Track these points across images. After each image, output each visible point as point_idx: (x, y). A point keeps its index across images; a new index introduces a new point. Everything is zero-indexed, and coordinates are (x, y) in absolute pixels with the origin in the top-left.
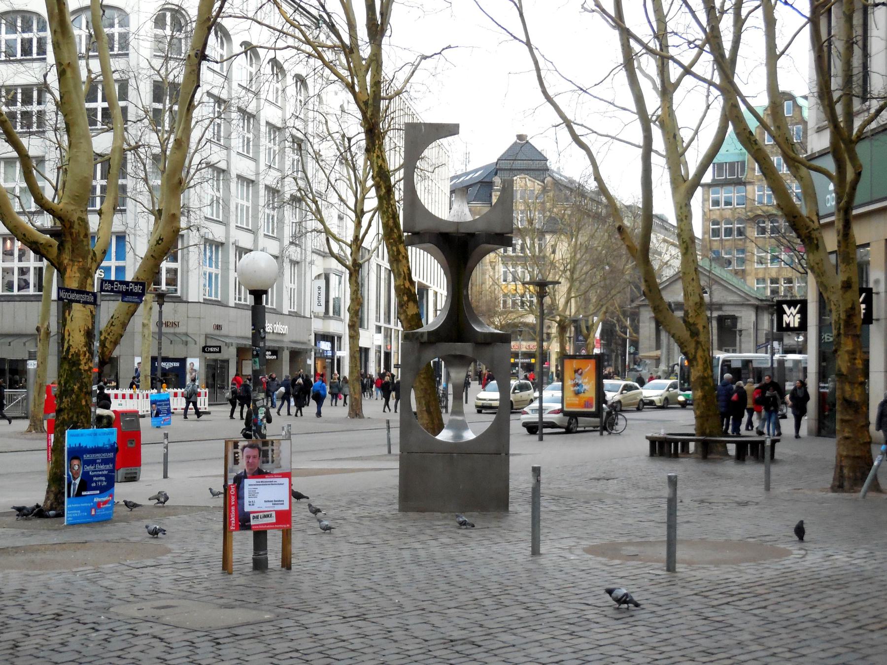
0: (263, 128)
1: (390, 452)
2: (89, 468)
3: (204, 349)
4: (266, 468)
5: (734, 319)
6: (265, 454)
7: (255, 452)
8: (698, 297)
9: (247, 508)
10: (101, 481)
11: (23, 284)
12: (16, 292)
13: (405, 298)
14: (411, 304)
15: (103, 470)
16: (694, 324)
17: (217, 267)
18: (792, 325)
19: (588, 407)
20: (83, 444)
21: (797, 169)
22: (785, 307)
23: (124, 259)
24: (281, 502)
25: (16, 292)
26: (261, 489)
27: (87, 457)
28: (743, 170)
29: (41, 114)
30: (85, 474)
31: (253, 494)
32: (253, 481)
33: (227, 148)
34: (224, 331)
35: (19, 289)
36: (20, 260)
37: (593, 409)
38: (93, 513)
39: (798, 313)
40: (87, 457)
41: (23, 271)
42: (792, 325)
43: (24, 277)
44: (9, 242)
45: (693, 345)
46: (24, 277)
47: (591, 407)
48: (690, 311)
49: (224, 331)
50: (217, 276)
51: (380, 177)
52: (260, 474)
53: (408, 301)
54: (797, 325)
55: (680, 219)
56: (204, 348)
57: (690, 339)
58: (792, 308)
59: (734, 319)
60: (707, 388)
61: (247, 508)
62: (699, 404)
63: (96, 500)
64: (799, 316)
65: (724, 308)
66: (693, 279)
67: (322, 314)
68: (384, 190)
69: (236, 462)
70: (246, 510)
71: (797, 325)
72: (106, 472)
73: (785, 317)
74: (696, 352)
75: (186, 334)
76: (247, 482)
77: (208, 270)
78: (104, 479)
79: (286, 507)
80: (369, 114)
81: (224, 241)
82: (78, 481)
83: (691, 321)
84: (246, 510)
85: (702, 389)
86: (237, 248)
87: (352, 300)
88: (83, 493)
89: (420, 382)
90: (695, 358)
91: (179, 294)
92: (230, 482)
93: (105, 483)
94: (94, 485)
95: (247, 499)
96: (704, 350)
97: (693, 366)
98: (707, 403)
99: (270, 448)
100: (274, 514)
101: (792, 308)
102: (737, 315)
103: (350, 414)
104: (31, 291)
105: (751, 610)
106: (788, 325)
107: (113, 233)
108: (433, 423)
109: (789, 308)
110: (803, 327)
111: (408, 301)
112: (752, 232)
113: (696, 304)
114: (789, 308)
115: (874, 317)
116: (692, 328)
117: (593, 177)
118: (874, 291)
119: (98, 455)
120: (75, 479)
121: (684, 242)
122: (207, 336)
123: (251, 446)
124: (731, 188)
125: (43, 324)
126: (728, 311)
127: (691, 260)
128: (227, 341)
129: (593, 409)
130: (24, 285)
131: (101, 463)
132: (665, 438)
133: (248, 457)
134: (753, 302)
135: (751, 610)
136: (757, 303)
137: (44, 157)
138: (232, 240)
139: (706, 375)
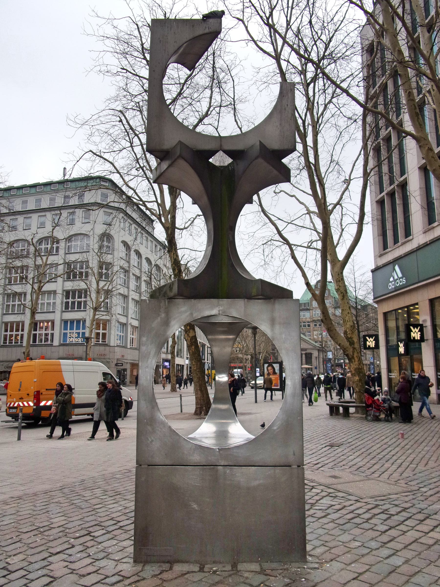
1: (182, 411)
3: (116, 365)
5: (311, 354)
8: (352, 322)
11: (46, 340)
12: (43, 343)
13: (188, 328)
14: (191, 331)
16: (351, 338)
17: (123, 333)
18: (371, 346)
19: (276, 386)
22: (367, 338)
25: (43, 343)
28: (308, 306)
33: (128, 288)
34: (125, 358)
35: (45, 342)
36: (46, 330)
37: (279, 387)
39: (374, 340)
41: (46, 335)
42: (371, 346)
43: (47, 337)
44: (42, 324)
45: (351, 350)
46: (47, 337)
47: (278, 386)
48: (348, 331)
49: (125, 358)
50: (123, 336)
51: (175, 265)
53: (190, 329)
54: (373, 346)
56: (116, 364)
57: (349, 347)
58: (371, 338)
59: (311, 354)
60: (361, 375)
62: (357, 384)
64: (374, 342)
65: (308, 350)
66: (348, 313)
67: (165, 352)
68: (177, 271)
71: (373, 346)
73: (368, 342)
74: (353, 354)
75: (109, 359)
77: (119, 334)
80: (169, 232)
81: (125, 322)
83: (349, 336)
85: (359, 375)
86: (131, 326)
87: (172, 342)
89: (196, 373)
90: (353, 357)
91: (107, 343)
96: (358, 353)
97: (352, 362)
98: (362, 383)
101: (371, 338)
102: (312, 352)
103: (171, 390)
104: (49, 342)
106: (369, 346)
108: (203, 397)
109: (369, 338)
110: (377, 346)
111: (190, 329)
113: (351, 326)
114: (369, 338)
115: (425, 339)
116: (350, 340)
117: (291, 257)
118: (424, 325)
121: (341, 293)
122: (118, 360)
124: (305, 311)
125: (26, 351)
126: (308, 351)
127: (346, 302)
128: (126, 361)
129: (279, 387)
130: (46, 340)
132: (402, 416)
134: (317, 348)
136: (319, 348)
137: (56, 291)
138: (129, 323)
139: (360, 367)
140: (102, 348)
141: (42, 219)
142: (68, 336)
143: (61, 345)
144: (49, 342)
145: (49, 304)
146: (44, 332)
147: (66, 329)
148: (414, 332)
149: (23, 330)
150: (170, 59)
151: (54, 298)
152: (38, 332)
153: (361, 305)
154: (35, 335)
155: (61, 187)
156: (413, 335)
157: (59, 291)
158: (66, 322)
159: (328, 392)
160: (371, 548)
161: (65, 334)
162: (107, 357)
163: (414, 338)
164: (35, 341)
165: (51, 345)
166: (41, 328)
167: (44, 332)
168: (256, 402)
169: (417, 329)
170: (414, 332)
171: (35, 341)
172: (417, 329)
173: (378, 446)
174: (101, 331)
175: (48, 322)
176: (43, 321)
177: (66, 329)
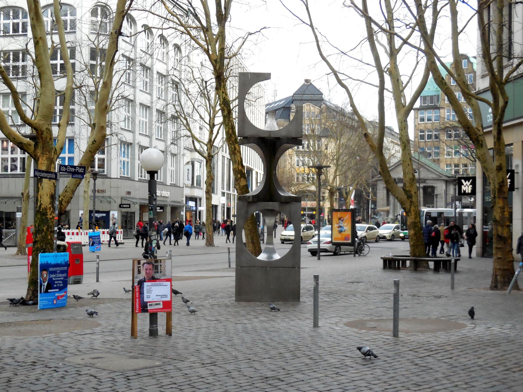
0: (155, 76)
1: (230, 266)
2: (52, 276)
3: (121, 206)
4: (157, 276)
5: (433, 188)
6: (156, 268)
7: (150, 266)
8: (412, 175)
9: (146, 300)
10: (60, 284)
11: (14, 167)
12: (9, 172)
13: (239, 176)
14: (242, 179)
15: (61, 277)
16: (409, 191)
17: (128, 157)
18: (467, 192)
19: (347, 240)
20: (49, 262)
21: (470, 99)
22: (463, 181)
23: (73, 153)
24: (166, 296)
25: (9, 172)
26: (154, 288)
27: (51, 269)
29: (24, 67)
30: (50, 279)
31: (149, 291)
32: (149, 284)
34: (132, 195)
35: (11, 170)
36: (12, 153)
37: (350, 241)
38: (55, 302)
39: (470, 184)
40: (51, 269)
41: (14, 160)
42: (467, 192)
43: (14, 163)
44: (5, 143)
45: (409, 203)
46: (14, 163)
47: (349, 240)
48: (407, 183)
49: (132, 195)
50: (128, 163)
51: (224, 105)
52: (153, 279)
53: (241, 177)
54: (470, 192)
55: (401, 129)
56: (120, 205)
57: (407, 200)
58: (467, 181)
59: (433, 188)
60: (417, 228)
61: (146, 300)
62: (412, 238)
63: (57, 295)
64: (471, 186)
65: (427, 182)
66: (409, 165)
68: (226, 112)
69: (139, 272)
70: (145, 301)
71: (470, 192)
72: (62, 278)
73: (463, 187)
74: (410, 208)
75: (110, 197)
76: (146, 284)
77: (123, 159)
78: (61, 282)
79: (168, 299)
80: (217, 67)
81: (132, 142)
82: (46, 284)
83: (407, 189)
84: (145, 301)
85: (414, 229)
86: (140, 146)
88: (49, 291)
89: (248, 225)
90: (410, 211)
91: (105, 173)
92: (136, 284)
93: (62, 285)
94: (55, 286)
95: (145, 294)
96: (415, 207)
97: (409, 216)
98: (417, 237)
99: (159, 264)
100: (161, 303)
101: (467, 181)
102: (435, 185)
103: (206, 244)
104: (18, 171)
105: (443, 359)
106: (465, 191)
107: (67, 137)
108: (255, 249)
109: (465, 182)
110: (473, 193)
111: (241, 177)
112: (444, 137)
113: (410, 179)
114: (465, 182)
115: (516, 187)
116: (408, 193)
117: (349, 105)
118: (515, 171)
119: (58, 268)
120: (44, 282)
121: (403, 143)
122: (122, 198)
123: (148, 263)
125: (25, 191)
126: (429, 183)
127: (407, 153)
128: (134, 201)
129: (350, 241)
130: (14, 168)
131: (60, 273)
132: (392, 258)
133: (146, 269)
134: (444, 178)
135: (443, 359)
136: (446, 178)
137: (26, 92)
138: (137, 142)
139: (416, 221)
148: (465, 185)
156: (463, 188)
163: (465, 191)
169: (469, 182)
170: (465, 185)
172: (469, 182)
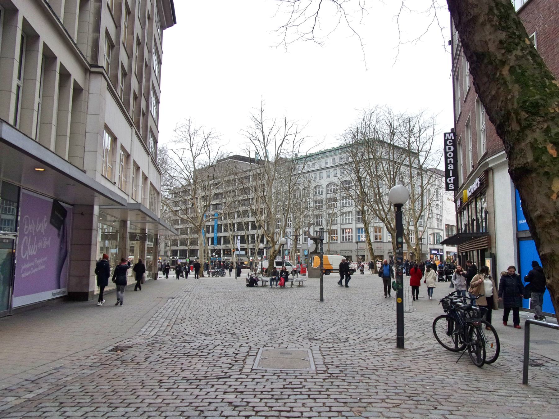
41: (349, 236)
104: (351, 241)
140: (379, 244)
141: (328, 173)
142: (360, 237)
143: (342, 243)
144: (351, 241)
145: (349, 219)
146: (348, 235)
147: (359, 233)
149: (337, 234)
150: (96, 161)
151: (352, 216)
152: (344, 235)
153: (171, 256)
154: (343, 237)
155: (323, 155)
157: (354, 211)
158: (359, 229)
159: (511, 312)
160: (257, 416)
161: (359, 236)
162: (382, 249)
164: (343, 240)
165: (337, 243)
166: (346, 233)
167: (348, 235)
168: (322, 300)
171: (343, 240)
173: (506, 391)
174: (378, 234)
175: (349, 229)
176: (347, 229)
177: (359, 233)
